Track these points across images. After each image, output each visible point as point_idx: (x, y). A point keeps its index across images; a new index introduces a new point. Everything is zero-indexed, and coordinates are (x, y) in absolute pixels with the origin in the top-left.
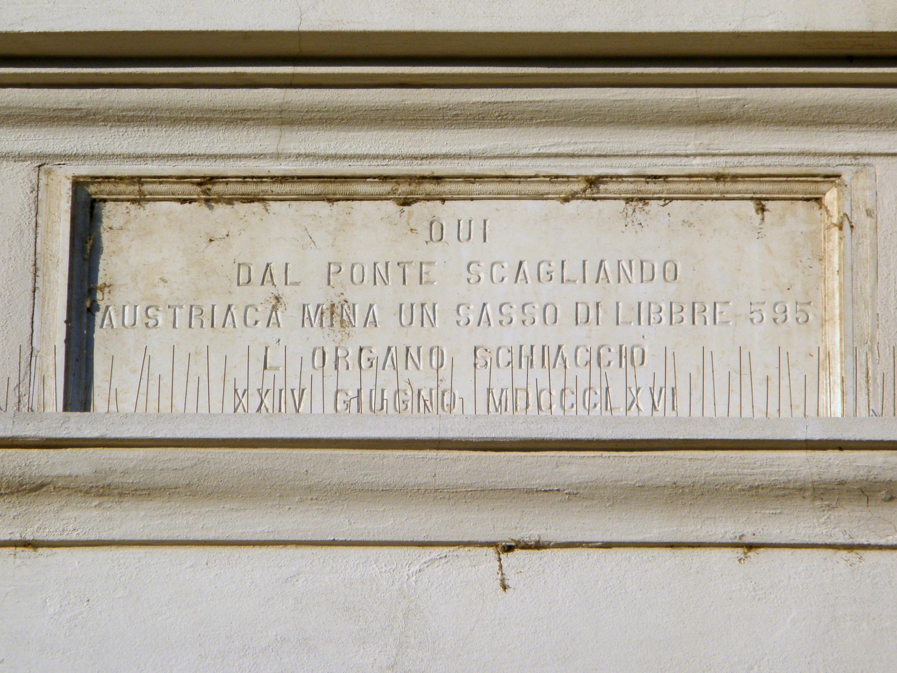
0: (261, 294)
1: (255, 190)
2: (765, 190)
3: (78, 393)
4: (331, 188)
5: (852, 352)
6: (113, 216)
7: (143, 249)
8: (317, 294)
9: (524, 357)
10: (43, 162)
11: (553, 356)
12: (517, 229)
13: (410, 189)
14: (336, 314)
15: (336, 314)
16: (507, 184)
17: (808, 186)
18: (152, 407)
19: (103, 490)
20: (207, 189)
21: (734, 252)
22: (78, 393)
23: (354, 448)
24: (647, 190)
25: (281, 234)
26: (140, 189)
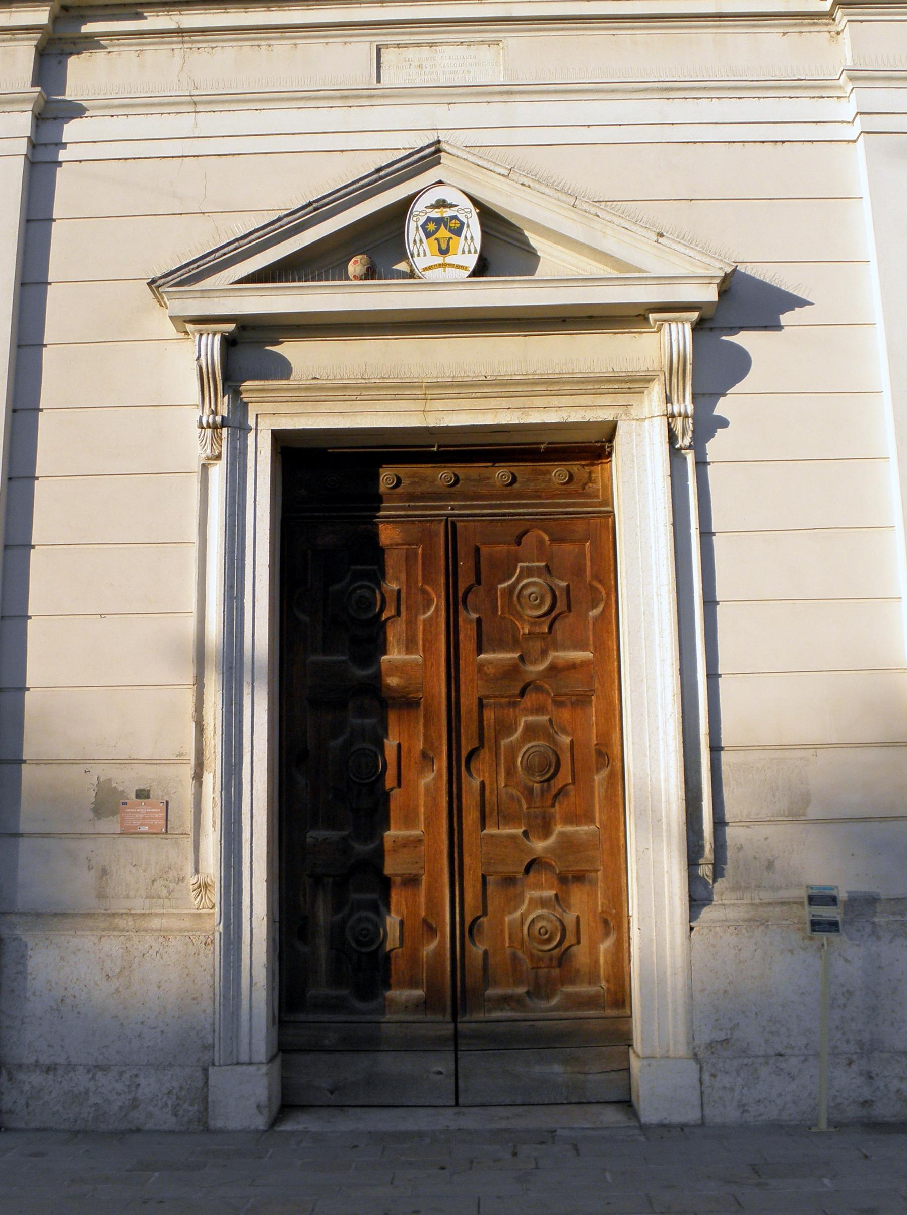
0: (408, 63)
1: (406, 46)
2: (490, 43)
3: (379, 81)
4: (418, 45)
5: (505, 70)
6: (383, 51)
7: (388, 56)
8: (417, 63)
9: (451, 72)
10: (371, 42)
11: (456, 72)
12: (449, 51)
13: (432, 45)
14: (420, 66)
15: (420, 66)
16: (447, 43)
17: (497, 43)
18: (204, 337)
19: (384, 96)
20: (398, 46)
21: (485, 53)
22: (379, 81)
23: (283, 495)
24: (470, 44)
25: (411, 53)
26: (387, 46)
